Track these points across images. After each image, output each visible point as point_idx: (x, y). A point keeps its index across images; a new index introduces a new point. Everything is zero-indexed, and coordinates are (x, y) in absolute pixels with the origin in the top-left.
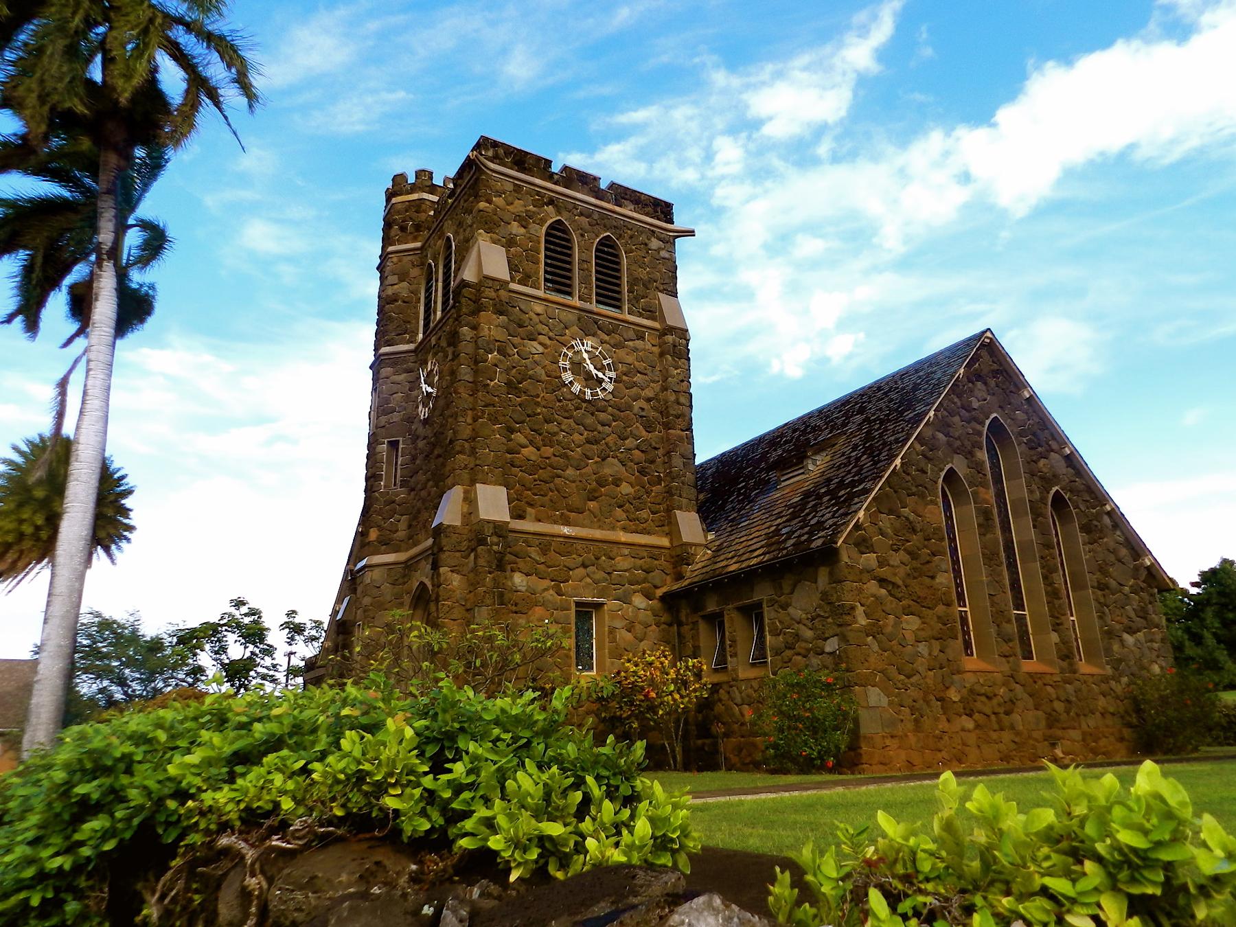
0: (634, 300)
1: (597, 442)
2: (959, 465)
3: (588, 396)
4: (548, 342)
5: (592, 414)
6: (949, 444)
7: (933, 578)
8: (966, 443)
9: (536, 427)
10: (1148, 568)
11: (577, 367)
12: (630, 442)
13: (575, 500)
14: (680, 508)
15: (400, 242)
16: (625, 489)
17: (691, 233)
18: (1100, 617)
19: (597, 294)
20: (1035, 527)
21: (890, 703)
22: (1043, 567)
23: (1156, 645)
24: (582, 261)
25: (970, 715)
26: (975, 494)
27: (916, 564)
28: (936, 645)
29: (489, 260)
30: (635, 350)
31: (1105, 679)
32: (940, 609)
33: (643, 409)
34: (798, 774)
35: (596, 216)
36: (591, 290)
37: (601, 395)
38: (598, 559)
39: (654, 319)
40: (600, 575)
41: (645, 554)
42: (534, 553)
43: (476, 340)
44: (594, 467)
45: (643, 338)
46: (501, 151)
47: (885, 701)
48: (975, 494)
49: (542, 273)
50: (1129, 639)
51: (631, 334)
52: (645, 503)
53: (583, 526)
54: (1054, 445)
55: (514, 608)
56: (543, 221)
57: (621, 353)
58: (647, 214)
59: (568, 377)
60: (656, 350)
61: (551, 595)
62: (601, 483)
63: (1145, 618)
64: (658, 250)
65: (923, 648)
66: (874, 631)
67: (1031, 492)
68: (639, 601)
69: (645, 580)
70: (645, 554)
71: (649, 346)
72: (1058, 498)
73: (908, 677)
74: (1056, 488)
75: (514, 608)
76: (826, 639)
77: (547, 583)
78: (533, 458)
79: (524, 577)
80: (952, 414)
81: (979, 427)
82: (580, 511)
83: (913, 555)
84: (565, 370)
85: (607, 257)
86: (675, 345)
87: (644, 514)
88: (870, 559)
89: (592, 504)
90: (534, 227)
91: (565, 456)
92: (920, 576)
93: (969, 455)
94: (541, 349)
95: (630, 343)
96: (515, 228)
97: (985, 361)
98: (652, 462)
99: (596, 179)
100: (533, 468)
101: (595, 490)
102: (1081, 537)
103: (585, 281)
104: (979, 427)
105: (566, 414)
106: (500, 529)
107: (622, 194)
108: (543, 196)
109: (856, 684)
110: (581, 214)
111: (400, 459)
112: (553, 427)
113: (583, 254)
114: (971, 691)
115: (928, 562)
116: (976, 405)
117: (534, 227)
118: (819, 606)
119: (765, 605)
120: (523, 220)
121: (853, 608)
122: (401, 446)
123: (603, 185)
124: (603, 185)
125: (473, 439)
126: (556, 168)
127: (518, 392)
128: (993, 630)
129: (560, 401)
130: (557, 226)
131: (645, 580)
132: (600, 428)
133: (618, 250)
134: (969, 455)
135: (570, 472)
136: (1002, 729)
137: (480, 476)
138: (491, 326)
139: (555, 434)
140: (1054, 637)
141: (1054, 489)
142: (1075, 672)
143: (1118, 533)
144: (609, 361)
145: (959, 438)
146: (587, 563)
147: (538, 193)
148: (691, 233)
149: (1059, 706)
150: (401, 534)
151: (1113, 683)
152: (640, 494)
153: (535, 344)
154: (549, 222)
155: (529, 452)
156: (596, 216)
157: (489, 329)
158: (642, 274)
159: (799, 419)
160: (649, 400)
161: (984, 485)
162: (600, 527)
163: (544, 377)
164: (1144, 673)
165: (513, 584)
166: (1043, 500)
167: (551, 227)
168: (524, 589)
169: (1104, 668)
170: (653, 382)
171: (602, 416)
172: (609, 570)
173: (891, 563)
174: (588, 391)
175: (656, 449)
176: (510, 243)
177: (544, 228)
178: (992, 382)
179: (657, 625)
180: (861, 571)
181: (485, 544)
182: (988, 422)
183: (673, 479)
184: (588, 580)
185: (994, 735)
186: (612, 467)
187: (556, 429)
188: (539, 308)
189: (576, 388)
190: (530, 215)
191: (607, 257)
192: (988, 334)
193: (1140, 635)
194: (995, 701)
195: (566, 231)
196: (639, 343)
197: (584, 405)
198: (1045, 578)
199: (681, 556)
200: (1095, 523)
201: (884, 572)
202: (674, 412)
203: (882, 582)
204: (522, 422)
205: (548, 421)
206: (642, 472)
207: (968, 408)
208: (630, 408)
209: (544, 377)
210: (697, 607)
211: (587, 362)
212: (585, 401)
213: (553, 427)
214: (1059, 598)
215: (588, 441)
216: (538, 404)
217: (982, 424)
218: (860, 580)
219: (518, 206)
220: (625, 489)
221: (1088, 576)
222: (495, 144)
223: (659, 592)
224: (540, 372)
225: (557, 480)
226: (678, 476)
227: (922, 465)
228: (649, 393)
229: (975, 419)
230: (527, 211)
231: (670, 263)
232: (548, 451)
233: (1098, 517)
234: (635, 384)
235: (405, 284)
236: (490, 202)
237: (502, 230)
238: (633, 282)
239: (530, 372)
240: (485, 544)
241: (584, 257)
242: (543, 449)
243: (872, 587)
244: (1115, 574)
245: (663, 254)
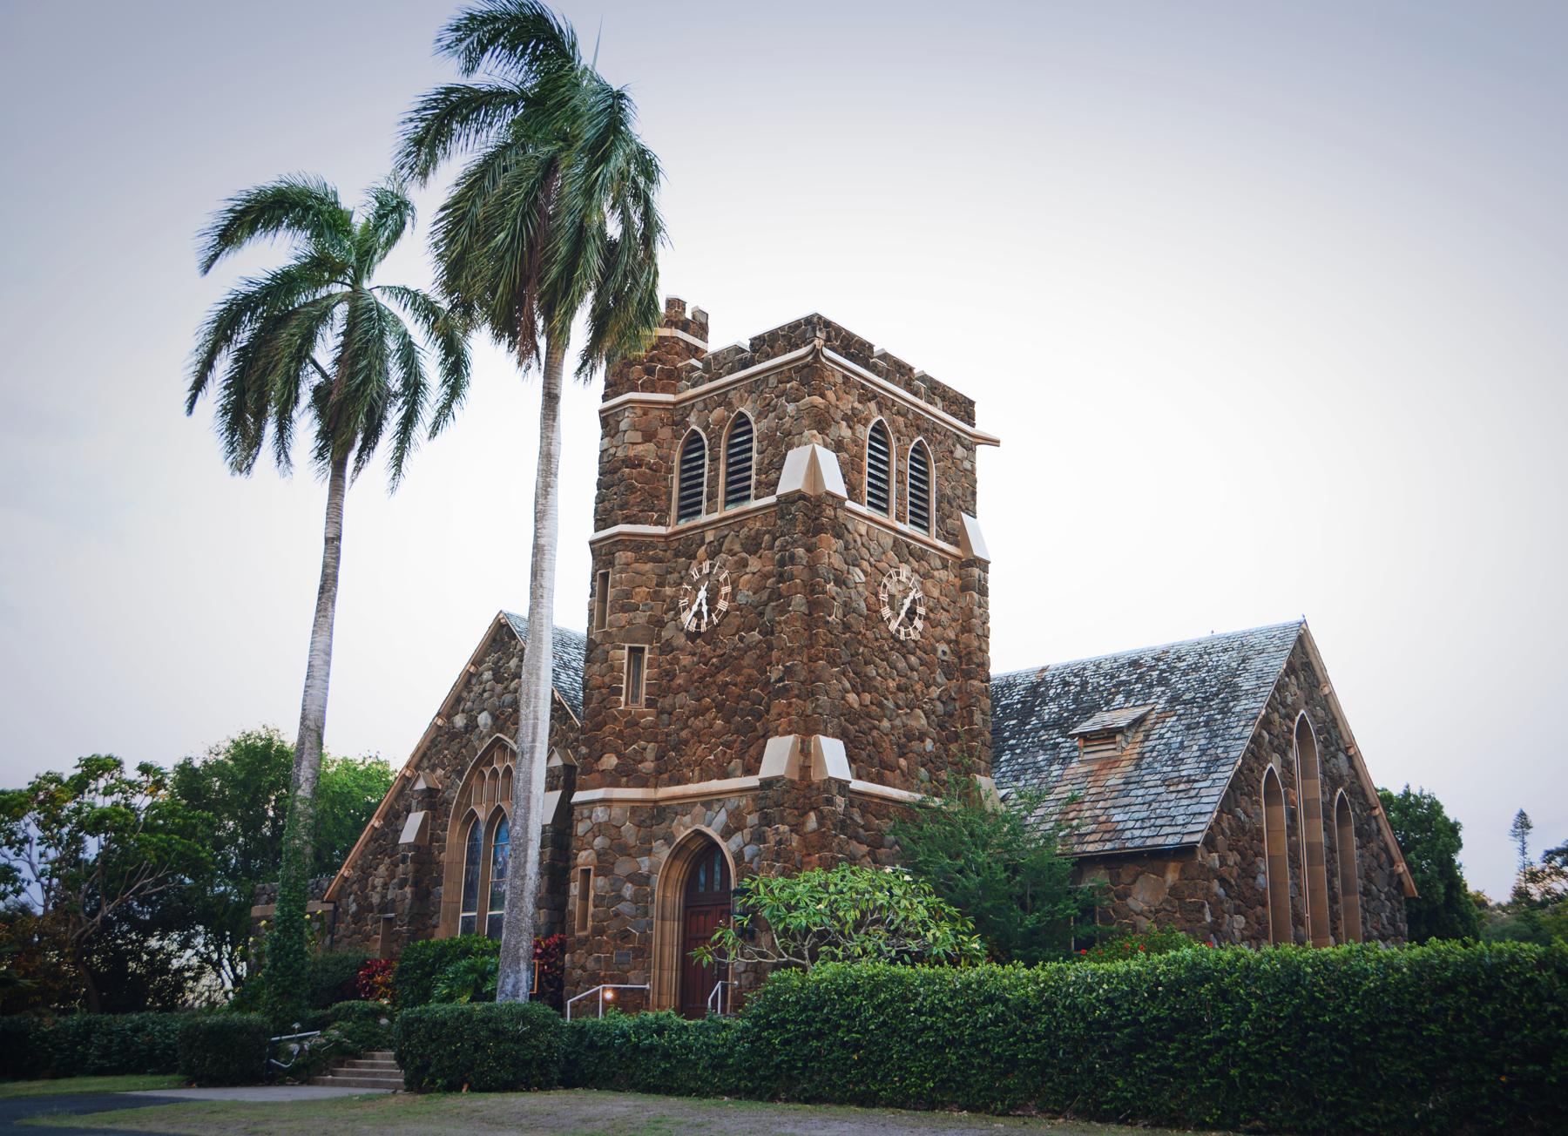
0: (941, 520)
6: (1270, 742)
15: (644, 389)
18: (1364, 923)
35: (910, 416)
39: (957, 544)
43: (812, 568)
48: (1286, 794)
51: (938, 563)
53: (894, 786)
57: (929, 583)
58: (954, 415)
60: (958, 582)
67: (1324, 793)
71: (952, 578)
86: (970, 575)
90: (859, 428)
93: (1283, 754)
96: (846, 432)
102: (1355, 841)
110: (898, 413)
111: (646, 672)
116: (1289, 700)
118: (1166, 901)
122: (647, 655)
134: (1283, 754)
135: (886, 724)
147: (863, 386)
150: (648, 766)
156: (910, 416)
162: (907, 789)
176: (838, 447)
183: (973, 739)
186: (920, 721)
201: (1224, 871)
206: (942, 727)
208: (935, 650)
212: (897, 640)
216: (860, 643)
217: (1293, 721)
220: (929, 745)
221: (1359, 881)
222: (828, 324)
225: (875, 733)
235: (651, 446)
238: (941, 498)
243: (1216, 887)
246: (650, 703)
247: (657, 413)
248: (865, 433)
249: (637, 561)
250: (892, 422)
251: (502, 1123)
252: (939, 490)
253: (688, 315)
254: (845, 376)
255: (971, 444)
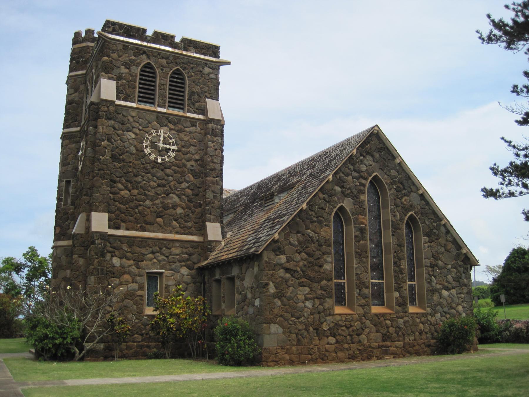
1: (164, 186)
2: (348, 204)
3: (159, 161)
4: (138, 132)
5: (162, 170)
6: (343, 192)
7: (321, 266)
8: (354, 190)
9: (128, 179)
10: (465, 254)
11: (153, 145)
12: (185, 185)
13: (149, 218)
14: (210, 221)
16: (179, 211)
17: (228, 63)
19: (169, 102)
20: (393, 235)
21: (284, 333)
22: (394, 257)
23: (463, 296)
24: (161, 85)
25: (334, 337)
26: (356, 219)
27: (311, 259)
28: (317, 302)
29: (107, 89)
30: (190, 132)
31: (424, 315)
32: (324, 282)
33: (192, 166)
34: (291, 363)
36: (165, 101)
37: (167, 160)
38: (161, 249)
40: (161, 257)
41: (189, 246)
42: (125, 248)
44: (161, 200)
45: (195, 126)
46: (117, 27)
47: (281, 330)
49: (137, 94)
50: (445, 293)
51: (188, 124)
52: (190, 218)
54: (414, 189)
55: (112, 275)
56: (139, 64)
57: (182, 135)
58: (203, 54)
59: (148, 151)
61: (134, 269)
62: (166, 207)
63: (458, 281)
64: (209, 74)
65: (309, 304)
66: (279, 295)
68: (184, 271)
69: (188, 260)
70: (189, 246)
72: (411, 218)
73: (298, 318)
74: (411, 213)
75: (112, 275)
76: (256, 299)
77: (132, 262)
78: (126, 196)
79: (119, 259)
80: (347, 175)
81: (363, 181)
82: (151, 224)
83: (309, 255)
84: (146, 147)
85: (177, 80)
87: (189, 224)
88: (283, 259)
89: (159, 220)
90: (133, 68)
91: (145, 195)
92: (313, 265)
93: (355, 197)
94: (133, 136)
95: (187, 129)
96: (124, 70)
97: (374, 145)
98: (196, 195)
99: (173, 37)
100: (124, 201)
101: (161, 212)
103: (162, 96)
104: (363, 181)
105: (147, 171)
106: (103, 236)
107: (188, 44)
108: (140, 50)
109: (264, 323)
110: (163, 58)
112: (139, 179)
113: (162, 81)
114: (336, 324)
115: (319, 258)
116: (364, 168)
117: (133, 68)
119: (235, 278)
120: (127, 65)
121: (267, 284)
123: (178, 40)
124: (178, 40)
125: (91, 188)
126: (149, 33)
127: (119, 161)
128: (356, 292)
129: (143, 164)
130: (148, 66)
131: (188, 260)
132: (166, 178)
133: (183, 75)
135: (148, 202)
136: (353, 343)
137: (94, 208)
138: (104, 126)
139: (140, 182)
140: (396, 294)
141: (410, 213)
142: (406, 312)
143: (449, 235)
144: (173, 140)
145: (350, 188)
146: (155, 251)
148: (228, 63)
149: (391, 330)
151: (429, 317)
152: (188, 213)
153: (130, 133)
154: (142, 65)
155: (125, 193)
157: (103, 128)
158: (197, 89)
159: (262, 181)
160: (196, 161)
161: (363, 213)
162: (162, 232)
163: (134, 151)
164: (453, 311)
165: (112, 263)
166: (401, 219)
167: (145, 66)
168: (118, 266)
169: (425, 309)
170: (200, 150)
171: (168, 171)
172: (167, 255)
173: (295, 260)
174: (160, 158)
175: (199, 188)
176: (118, 78)
177: (140, 68)
178: (377, 155)
179: (195, 283)
180: (275, 265)
181: (95, 244)
182: (370, 178)
183: (207, 205)
184: (155, 260)
185: (346, 346)
187: (140, 180)
188: (134, 114)
189: (152, 157)
190: (132, 61)
191: (177, 80)
192: (376, 128)
193: (453, 291)
194: (351, 329)
195: (152, 68)
196: (192, 129)
197: (158, 165)
198: (395, 263)
199: (207, 247)
200: (435, 231)
201: (291, 265)
202: (210, 166)
203: (287, 270)
204: (121, 177)
205: (136, 176)
206: (190, 201)
207: (358, 171)
208: (185, 166)
209: (134, 151)
210: (212, 274)
211: (161, 143)
213: (139, 179)
214: (402, 274)
215: (159, 186)
216: (130, 167)
218: (274, 270)
219: (125, 58)
220: (179, 211)
222: (114, 24)
223: (196, 266)
224: (133, 149)
226: (210, 203)
227: (323, 205)
228: (197, 157)
229: (362, 177)
230: (129, 59)
231: (215, 81)
232: (135, 192)
233: (438, 228)
234: (189, 152)
235: (77, 94)
236: (108, 56)
237: (116, 71)
238: (192, 94)
239: (128, 149)
240: (95, 244)
241: (162, 82)
242: (132, 191)
244: (443, 259)
245: (212, 76)
246: (73, 204)
247: (79, 79)
248: (137, 71)
249: (70, 144)
250: (156, 63)
251: (294, 387)
252: (190, 90)
253: (96, 35)
254: (124, 46)
255: (216, 67)
